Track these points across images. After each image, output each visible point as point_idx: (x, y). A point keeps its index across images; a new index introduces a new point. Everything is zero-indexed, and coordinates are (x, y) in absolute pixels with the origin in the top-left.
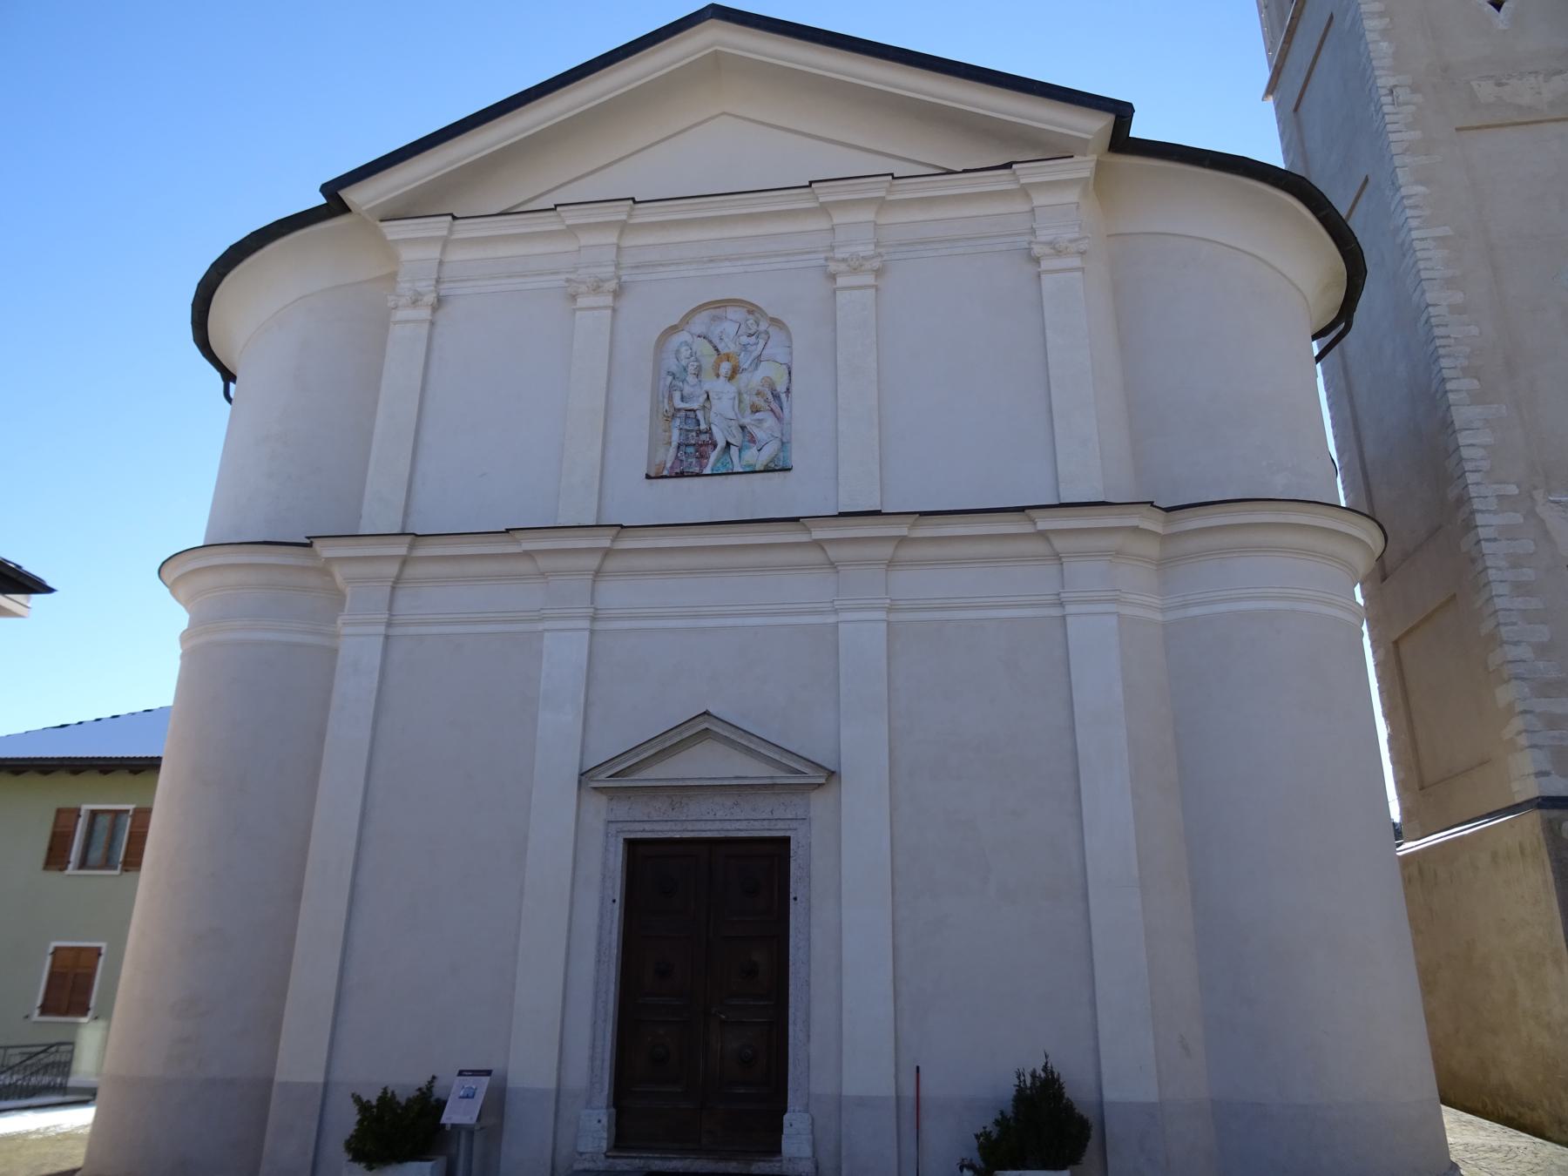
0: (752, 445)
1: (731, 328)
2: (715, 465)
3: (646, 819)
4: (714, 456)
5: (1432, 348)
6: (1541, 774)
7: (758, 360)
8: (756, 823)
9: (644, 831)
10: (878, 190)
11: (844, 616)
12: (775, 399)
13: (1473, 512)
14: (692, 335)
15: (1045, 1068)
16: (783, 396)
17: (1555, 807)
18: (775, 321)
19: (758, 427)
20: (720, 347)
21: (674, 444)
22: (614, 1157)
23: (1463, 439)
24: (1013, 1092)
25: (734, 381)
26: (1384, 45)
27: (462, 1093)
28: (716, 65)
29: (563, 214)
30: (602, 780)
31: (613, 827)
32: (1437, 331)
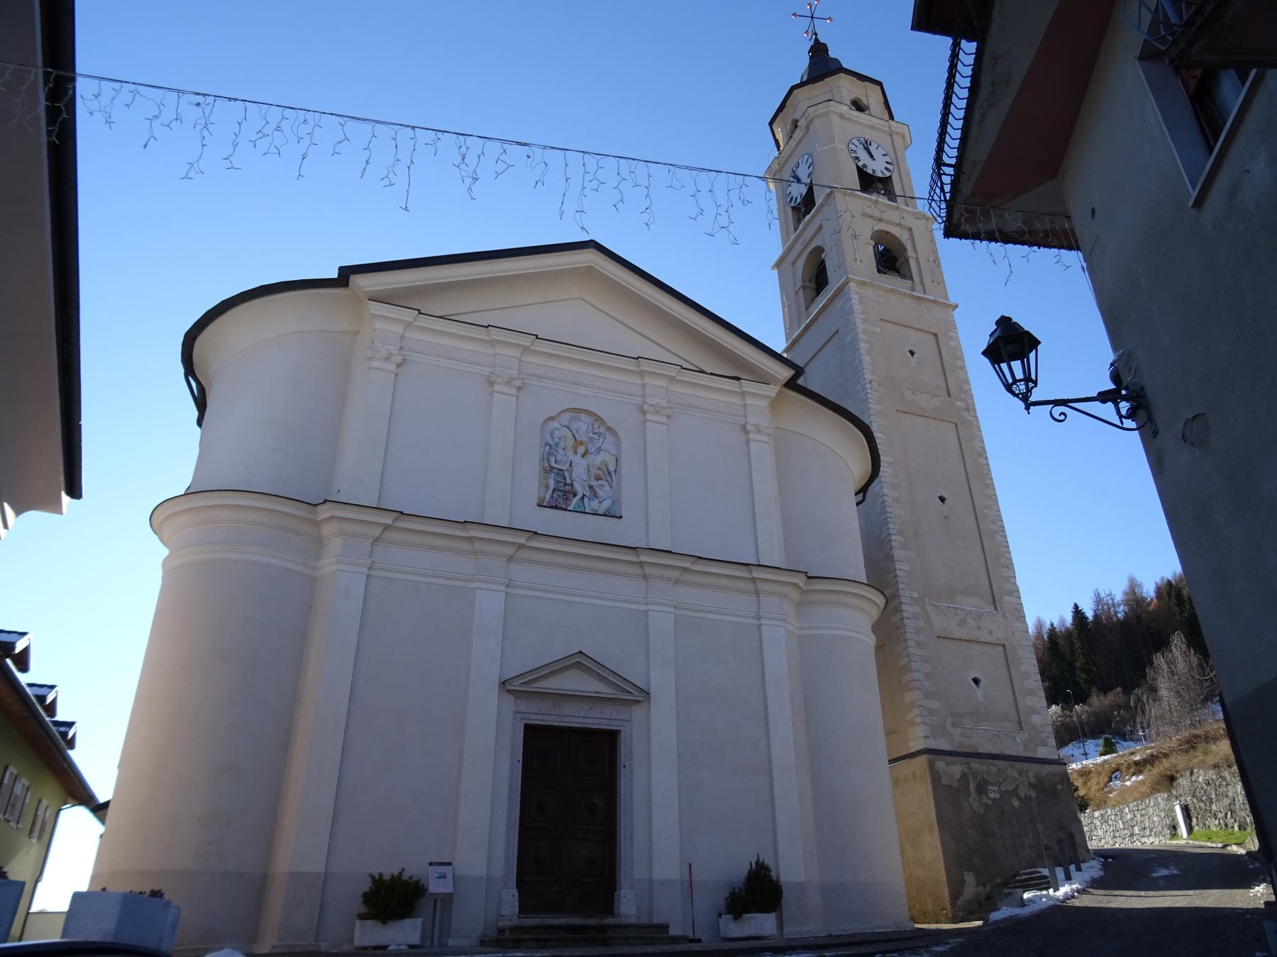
0: (595, 498)
1: (583, 427)
2: (574, 506)
3: (538, 712)
4: (575, 500)
5: (884, 517)
6: (926, 737)
7: (599, 449)
8: (603, 721)
9: (537, 720)
10: (672, 372)
11: (651, 607)
12: (608, 474)
13: (901, 603)
14: (561, 425)
15: (757, 863)
16: (613, 473)
17: (932, 754)
18: (609, 429)
19: (600, 489)
20: (576, 436)
21: (552, 488)
22: (523, 918)
23: (898, 565)
24: (746, 875)
25: (586, 457)
26: (868, 358)
27: (436, 875)
28: (589, 272)
29: (743, 384)
30: (516, 686)
31: (519, 716)
32: (888, 509)
